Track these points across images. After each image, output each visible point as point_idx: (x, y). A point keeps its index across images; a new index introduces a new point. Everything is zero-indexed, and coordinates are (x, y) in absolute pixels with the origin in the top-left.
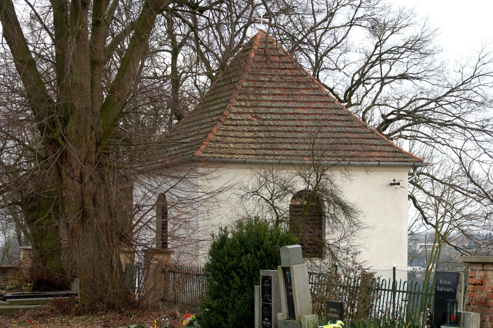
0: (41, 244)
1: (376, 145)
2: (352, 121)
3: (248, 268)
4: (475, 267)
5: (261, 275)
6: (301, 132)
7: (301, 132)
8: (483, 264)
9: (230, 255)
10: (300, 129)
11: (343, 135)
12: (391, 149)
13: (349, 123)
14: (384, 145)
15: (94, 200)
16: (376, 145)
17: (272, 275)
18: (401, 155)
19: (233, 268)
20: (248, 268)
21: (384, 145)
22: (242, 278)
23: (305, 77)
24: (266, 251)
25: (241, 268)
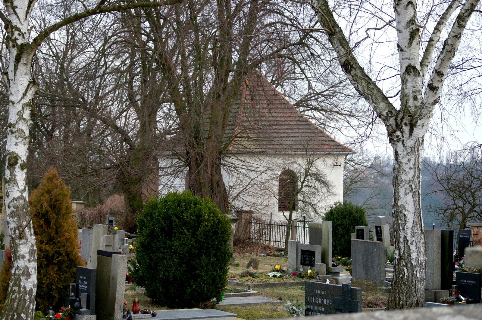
0: (133, 203)
1: (325, 141)
2: (309, 125)
3: (346, 224)
4: (473, 228)
5: (356, 228)
6: (282, 133)
7: (282, 133)
8: (478, 227)
9: (337, 219)
10: (281, 131)
11: (306, 135)
12: (334, 144)
13: (308, 127)
14: (330, 141)
15: (218, 184)
16: (325, 141)
17: (364, 229)
18: (340, 147)
19: (339, 225)
20: (346, 224)
21: (330, 141)
22: (343, 230)
23: (278, 96)
24: (353, 217)
25: (342, 225)
